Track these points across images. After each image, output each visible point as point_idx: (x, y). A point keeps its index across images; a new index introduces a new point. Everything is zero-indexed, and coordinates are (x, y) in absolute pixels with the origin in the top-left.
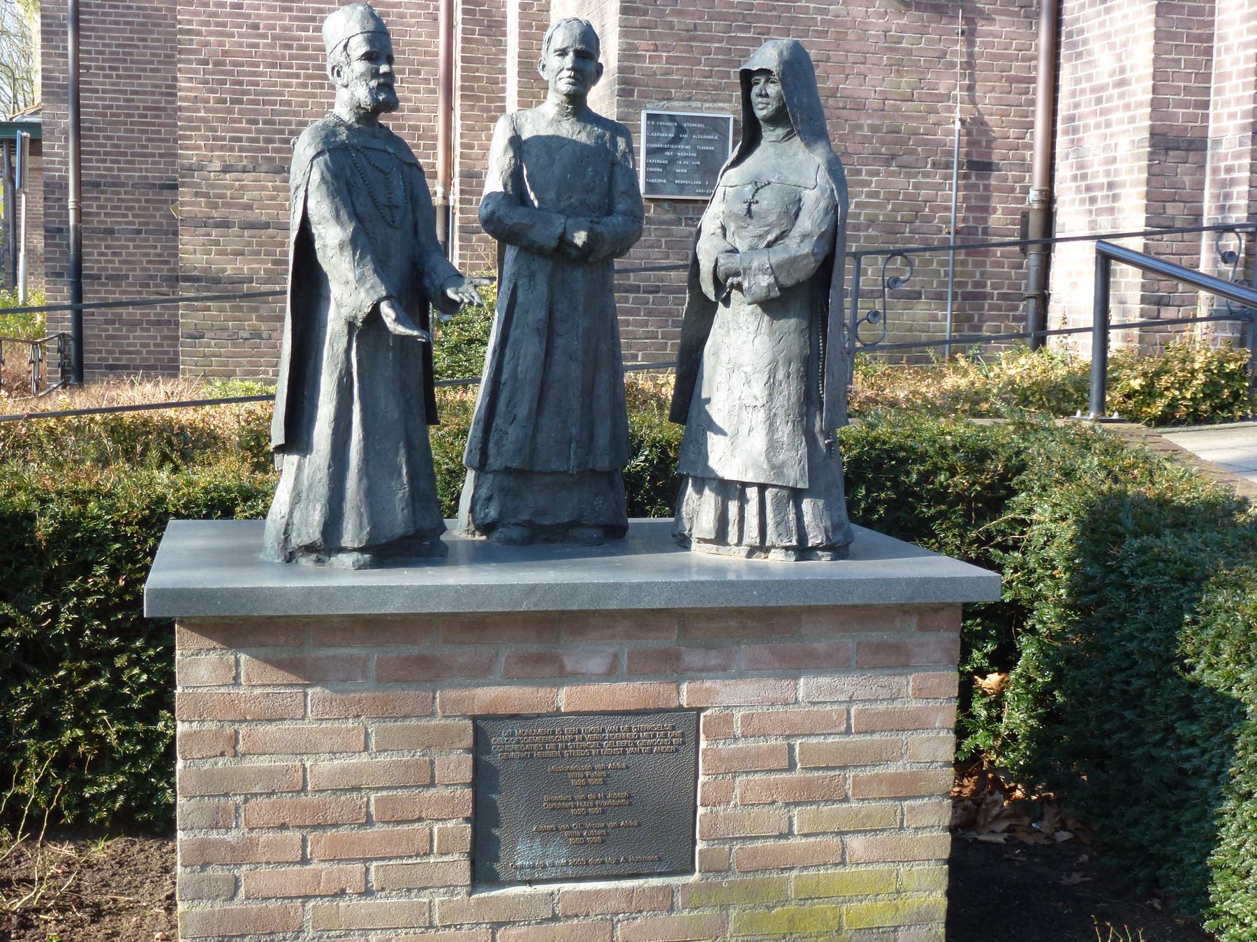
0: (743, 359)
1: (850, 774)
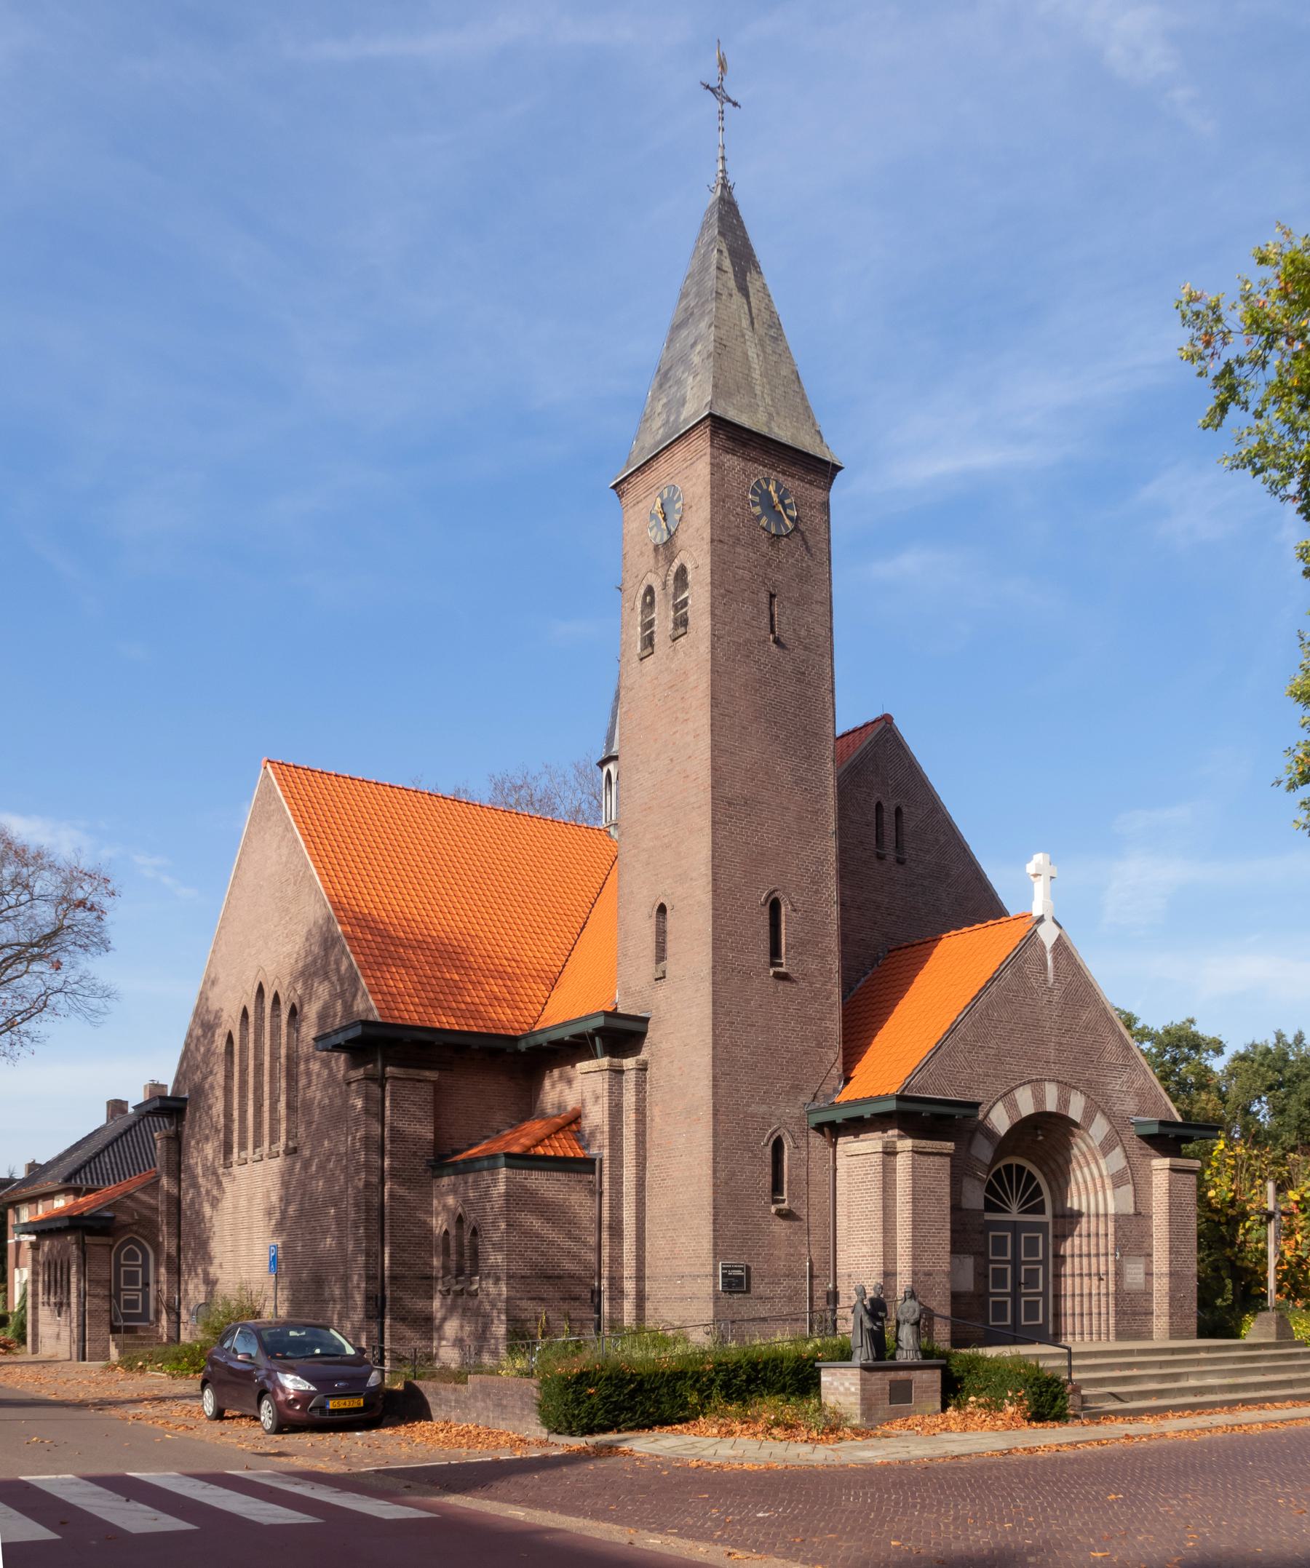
0: (906, 1333)
1: (1009, 1235)
